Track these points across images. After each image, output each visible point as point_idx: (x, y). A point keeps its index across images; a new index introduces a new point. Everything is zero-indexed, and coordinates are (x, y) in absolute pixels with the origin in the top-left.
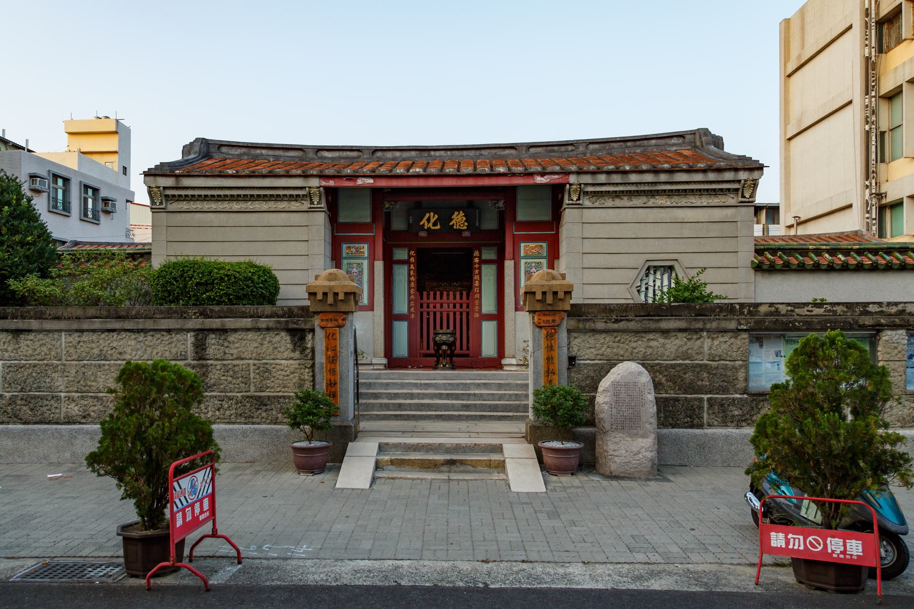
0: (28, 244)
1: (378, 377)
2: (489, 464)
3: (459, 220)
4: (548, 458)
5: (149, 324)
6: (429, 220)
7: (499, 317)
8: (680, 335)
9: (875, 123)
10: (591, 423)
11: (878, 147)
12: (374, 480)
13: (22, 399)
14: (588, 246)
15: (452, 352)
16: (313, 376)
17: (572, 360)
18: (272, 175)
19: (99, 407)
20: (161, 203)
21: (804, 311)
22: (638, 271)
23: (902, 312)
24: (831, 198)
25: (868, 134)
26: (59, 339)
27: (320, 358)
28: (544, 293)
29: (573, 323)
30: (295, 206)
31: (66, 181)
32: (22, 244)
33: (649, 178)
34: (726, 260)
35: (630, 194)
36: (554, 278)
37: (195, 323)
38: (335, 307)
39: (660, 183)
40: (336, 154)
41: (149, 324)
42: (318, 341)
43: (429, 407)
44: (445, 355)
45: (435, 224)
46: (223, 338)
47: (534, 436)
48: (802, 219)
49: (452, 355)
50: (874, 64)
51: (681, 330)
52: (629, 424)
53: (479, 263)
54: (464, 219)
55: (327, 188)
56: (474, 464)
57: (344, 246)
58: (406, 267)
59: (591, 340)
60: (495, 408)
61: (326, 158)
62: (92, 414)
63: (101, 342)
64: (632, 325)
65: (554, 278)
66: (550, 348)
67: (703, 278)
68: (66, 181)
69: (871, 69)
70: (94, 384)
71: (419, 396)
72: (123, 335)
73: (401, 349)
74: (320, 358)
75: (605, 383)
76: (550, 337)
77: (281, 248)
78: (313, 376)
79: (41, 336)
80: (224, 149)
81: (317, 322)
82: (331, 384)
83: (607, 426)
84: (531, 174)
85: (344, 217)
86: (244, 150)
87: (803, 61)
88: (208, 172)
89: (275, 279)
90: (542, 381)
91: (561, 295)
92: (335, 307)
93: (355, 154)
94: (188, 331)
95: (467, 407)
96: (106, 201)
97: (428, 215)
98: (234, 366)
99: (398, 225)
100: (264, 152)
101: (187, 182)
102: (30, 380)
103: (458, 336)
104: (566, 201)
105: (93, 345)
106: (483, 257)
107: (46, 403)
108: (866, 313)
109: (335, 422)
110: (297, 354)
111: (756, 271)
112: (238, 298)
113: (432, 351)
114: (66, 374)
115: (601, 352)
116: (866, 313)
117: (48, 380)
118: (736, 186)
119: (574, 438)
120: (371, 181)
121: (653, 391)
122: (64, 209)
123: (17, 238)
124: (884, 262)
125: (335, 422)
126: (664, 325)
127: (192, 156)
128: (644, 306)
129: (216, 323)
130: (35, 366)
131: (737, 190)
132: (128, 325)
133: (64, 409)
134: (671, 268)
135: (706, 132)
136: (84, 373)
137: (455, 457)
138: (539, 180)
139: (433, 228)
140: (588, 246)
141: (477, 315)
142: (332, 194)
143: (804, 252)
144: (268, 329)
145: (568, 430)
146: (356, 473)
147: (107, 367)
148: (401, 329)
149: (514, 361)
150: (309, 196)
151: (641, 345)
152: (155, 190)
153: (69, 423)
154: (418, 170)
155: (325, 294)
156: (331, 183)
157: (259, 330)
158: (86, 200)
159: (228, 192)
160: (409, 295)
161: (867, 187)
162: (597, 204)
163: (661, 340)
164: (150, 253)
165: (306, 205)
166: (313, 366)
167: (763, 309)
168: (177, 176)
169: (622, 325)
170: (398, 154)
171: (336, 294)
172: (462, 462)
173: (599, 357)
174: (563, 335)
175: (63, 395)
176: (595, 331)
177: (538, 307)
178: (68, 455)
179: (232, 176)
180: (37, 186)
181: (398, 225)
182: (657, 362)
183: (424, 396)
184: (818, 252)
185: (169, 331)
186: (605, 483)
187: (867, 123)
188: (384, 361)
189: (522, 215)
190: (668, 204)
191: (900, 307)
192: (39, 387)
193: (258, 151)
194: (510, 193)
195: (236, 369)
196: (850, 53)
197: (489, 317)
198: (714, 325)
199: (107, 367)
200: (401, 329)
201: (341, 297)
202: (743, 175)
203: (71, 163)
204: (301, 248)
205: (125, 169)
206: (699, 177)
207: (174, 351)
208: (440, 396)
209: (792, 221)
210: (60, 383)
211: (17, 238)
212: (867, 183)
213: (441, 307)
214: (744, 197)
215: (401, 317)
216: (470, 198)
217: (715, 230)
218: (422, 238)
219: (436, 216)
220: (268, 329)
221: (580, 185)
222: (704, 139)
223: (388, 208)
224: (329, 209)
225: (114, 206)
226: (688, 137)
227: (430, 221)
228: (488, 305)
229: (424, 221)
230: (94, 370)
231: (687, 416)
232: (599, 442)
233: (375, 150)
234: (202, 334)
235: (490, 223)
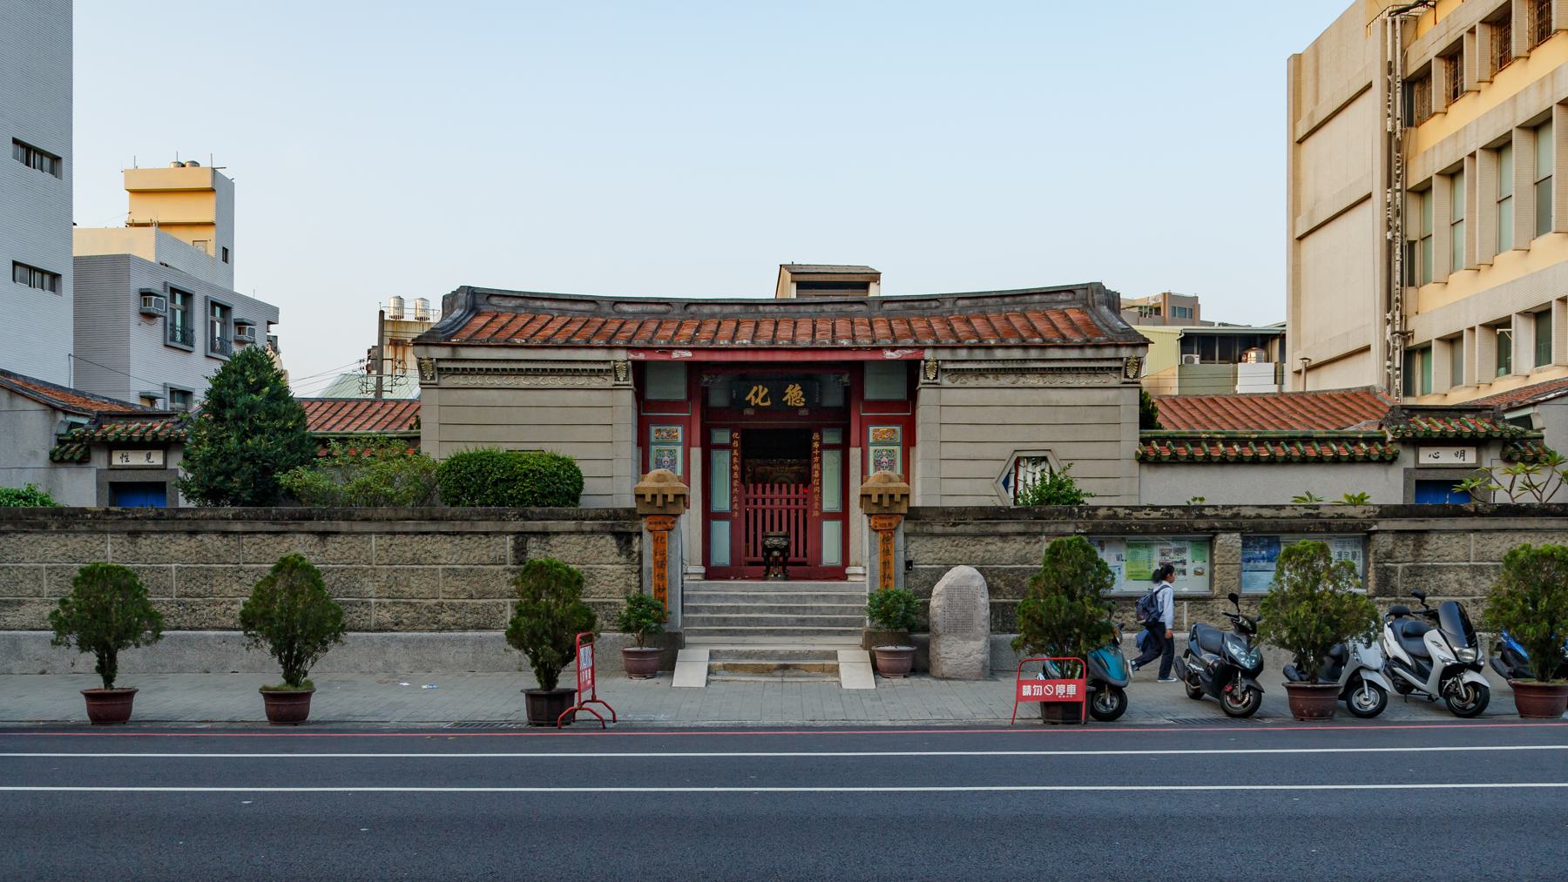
0: (287, 430)
1: (697, 588)
2: (823, 669)
3: (794, 395)
4: (882, 662)
5: (466, 527)
6: (756, 395)
7: (843, 516)
8: (1019, 539)
9: (1402, 229)
10: (926, 629)
11: (1404, 264)
12: (708, 682)
14: (947, 433)
15: (786, 559)
16: (641, 581)
17: (909, 564)
18: (568, 345)
19: (412, 614)
20: (433, 378)
21: (1141, 515)
23: (1237, 515)
24: (1347, 334)
25: (1390, 244)
26: (369, 542)
27: (648, 563)
28: (880, 496)
29: (910, 526)
30: (596, 382)
31: (187, 297)
32: (285, 430)
33: (1017, 354)
34: (1106, 450)
35: (996, 372)
36: (890, 480)
37: (516, 525)
38: (661, 510)
40: (639, 308)
41: (466, 527)
42: (646, 545)
43: (759, 621)
44: (776, 563)
45: (764, 400)
47: (871, 640)
49: (785, 563)
50: (1399, 143)
51: (1019, 534)
52: (961, 627)
55: (634, 362)
56: (807, 669)
57: (653, 429)
58: (727, 454)
59: (929, 544)
60: (835, 622)
61: (625, 313)
64: (970, 529)
65: (890, 480)
66: (886, 552)
67: (1071, 473)
68: (187, 297)
69: (1395, 151)
71: (745, 610)
72: (438, 537)
73: (722, 555)
74: (648, 563)
75: (939, 587)
76: (886, 540)
77: (581, 433)
78: (641, 581)
80: (494, 301)
81: (644, 525)
82: (660, 590)
83: (940, 629)
84: (880, 349)
85: (652, 394)
86: (519, 302)
88: (478, 331)
89: (577, 471)
90: (878, 586)
91: (897, 498)
92: (661, 510)
93: (662, 308)
94: (508, 533)
96: (240, 325)
99: (718, 399)
100: (546, 304)
101: (465, 353)
103: (793, 538)
104: (922, 380)
108: (1202, 516)
109: (666, 628)
110: (623, 559)
112: (543, 496)
113: (760, 558)
116: (1202, 516)
118: (1118, 364)
119: (909, 643)
120: (689, 354)
121: (987, 595)
122: (184, 341)
123: (278, 424)
125: (666, 628)
126: (1002, 528)
127: (457, 313)
129: (537, 526)
131: (1119, 369)
132: (444, 527)
134: (1044, 459)
135: (1098, 288)
138: (889, 355)
140: (947, 433)
142: (639, 369)
143: (1195, 441)
144: (592, 532)
145: (902, 635)
146: (691, 671)
148: (722, 530)
149: (860, 570)
150: (614, 371)
151: (978, 549)
153: (380, 630)
156: (641, 356)
157: (583, 533)
158: (213, 324)
159: (515, 366)
160: (732, 487)
161: (1388, 321)
165: (610, 382)
166: (640, 571)
167: (1101, 512)
168: (453, 346)
169: (960, 528)
170: (717, 309)
171: (665, 496)
172: (796, 667)
174: (899, 539)
176: (933, 535)
177: (875, 510)
178: (380, 664)
179: (521, 347)
180: (152, 308)
181: (718, 399)
183: (753, 609)
184: (1211, 442)
185: (487, 534)
186: (934, 682)
187: (1389, 228)
188: (702, 570)
189: (870, 394)
190: (1041, 384)
191: (1235, 510)
193: (538, 303)
194: (857, 368)
196: (1366, 126)
197: (831, 516)
198: (1052, 528)
200: (722, 530)
201: (671, 499)
202: (1125, 353)
203: (144, 247)
204: (604, 433)
205: (225, 251)
206: (1075, 354)
208: (771, 610)
209: (1299, 366)
210: (370, 588)
211: (278, 424)
212: (1389, 316)
213: (772, 502)
215: (721, 516)
216: (808, 373)
217: (1094, 415)
218: (748, 418)
220: (592, 532)
222: (1096, 296)
225: (252, 332)
226: (1080, 293)
227: (758, 395)
228: (830, 502)
229: (751, 396)
230: (406, 574)
232: (932, 646)
233: (689, 304)
234: (522, 537)
235: (833, 399)
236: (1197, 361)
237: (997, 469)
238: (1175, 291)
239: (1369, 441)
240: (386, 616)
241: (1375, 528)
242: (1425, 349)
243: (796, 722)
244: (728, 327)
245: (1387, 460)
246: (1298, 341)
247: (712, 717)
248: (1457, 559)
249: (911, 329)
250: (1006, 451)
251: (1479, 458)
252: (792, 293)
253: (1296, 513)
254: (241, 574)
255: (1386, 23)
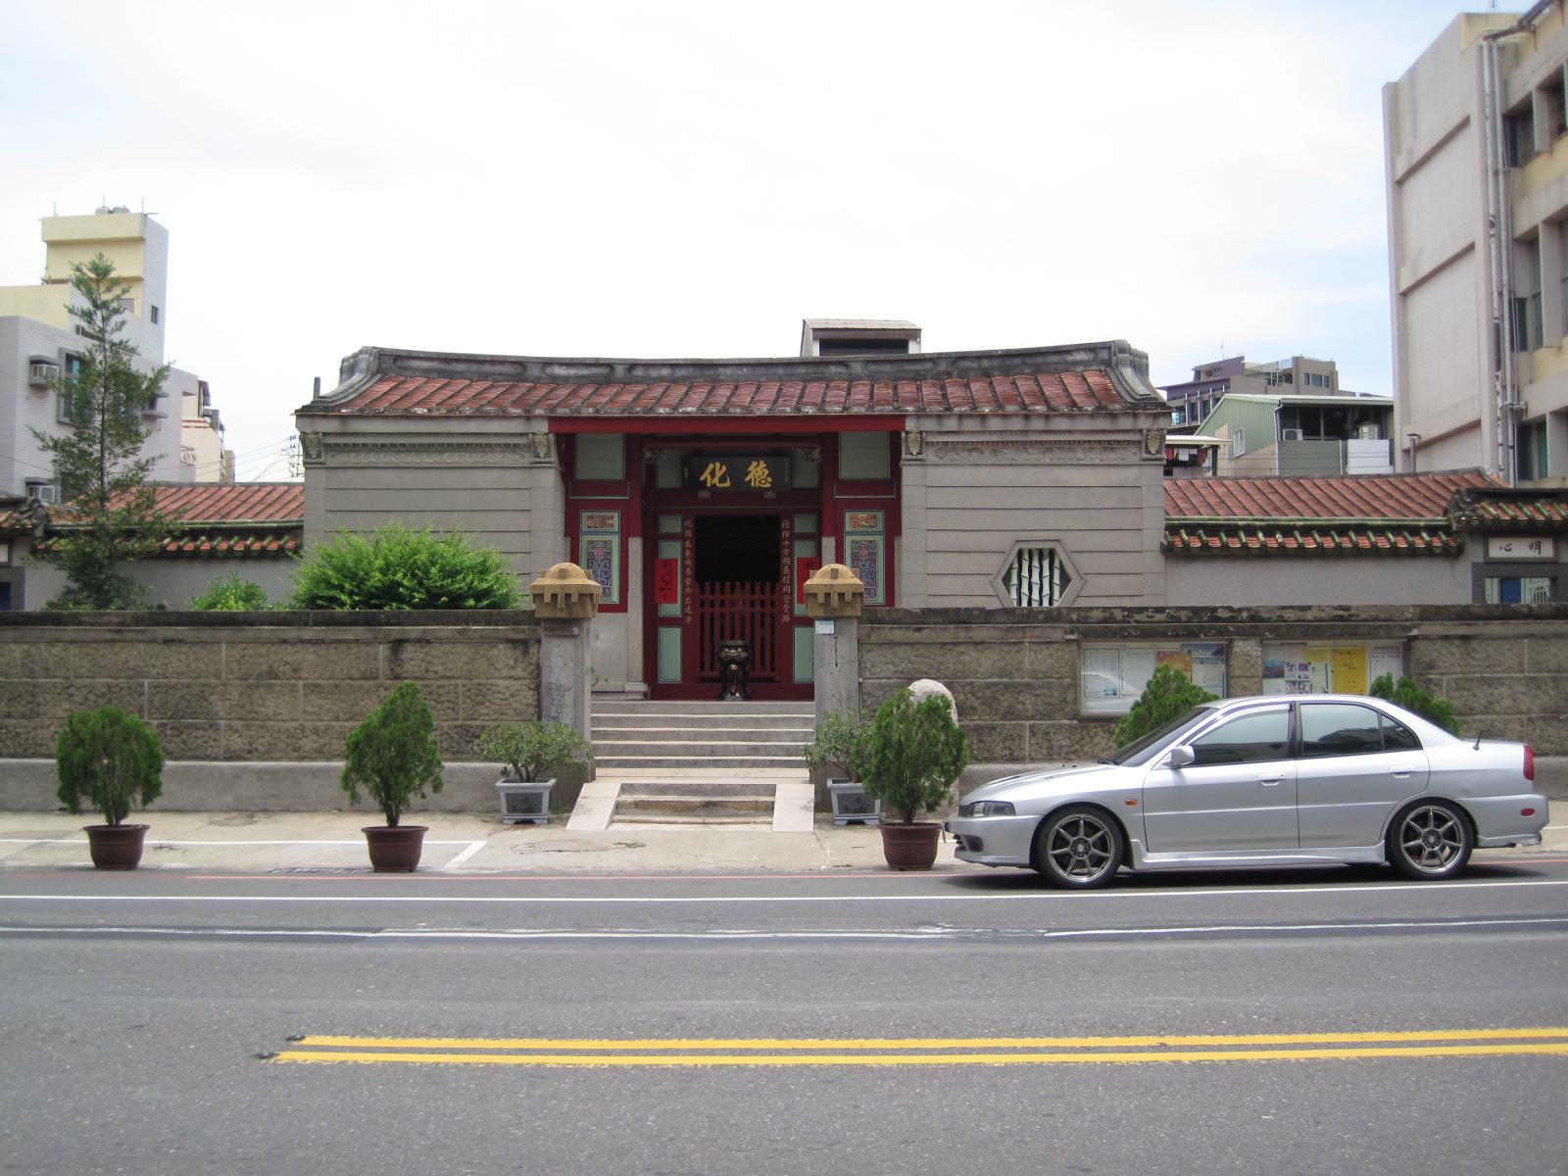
13: (172, 729)
20: (319, 455)
22: (1005, 556)
26: (219, 652)
30: (510, 459)
34: (1127, 541)
39: (1032, 431)
45: (722, 480)
46: (425, 650)
48: (1424, 439)
53: (790, 539)
54: (767, 472)
57: (585, 515)
62: (260, 748)
63: (271, 655)
70: (262, 709)
73: (671, 668)
79: (196, 648)
85: (585, 471)
87: (1415, 160)
95: (755, 750)
97: (711, 466)
98: (439, 687)
102: (183, 704)
104: (904, 456)
105: (261, 660)
106: (797, 531)
107: (201, 733)
111: (1166, 557)
114: (228, 696)
115: (900, 668)
117: (205, 704)
118: (1137, 437)
124: (1332, 545)
128: (1008, 612)
130: (188, 686)
131: (1139, 442)
133: (224, 742)
136: (249, 696)
137: (714, 799)
139: (718, 485)
141: (786, 618)
147: (278, 688)
150: (531, 447)
152: (311, 436)
154: (689, 409)
155: (554, 596)
159: (402, 440)
162: (946, 460)
163: (974, 654)
164: (300, 528)
168: (343, 417)
170: (665, 372)
173: (897, 675)
175: (222, 722)
182: (969, 680)
184: (1251, 531)
192: (195, 713)
195: (441, 691)
199: (278, 688)
200: (671, 641)
202: (1144, 423)
204: (521, 522)
205: (155, 310)
207: (363, 667)
209: (1407, 444)
214: (1149, 452)
219: (724, 468)
221: (921, 433)
223: (649, 459)
224: (561, 463)
227: (715, 474)
229: (706, 475)
231: (1005, 748)
236: (1300, 436)
237: (996, 564)
238: (1307, 355)
239: (1433, 530)
240: (237, 742)
241: (1415, 632)
242: (1540, 425)
243: (711, 867)
244: (770, 391)
245: (1452, 554)
246: (1408, 413)
247: (616, 861)
248: (1510, 669)
249: (945, 396)
250: (1006, 541)
251: (1556, 550)
252: (815, 351)
253: (1323, 615)
254: (72, 690)
255: (1481, 48)
